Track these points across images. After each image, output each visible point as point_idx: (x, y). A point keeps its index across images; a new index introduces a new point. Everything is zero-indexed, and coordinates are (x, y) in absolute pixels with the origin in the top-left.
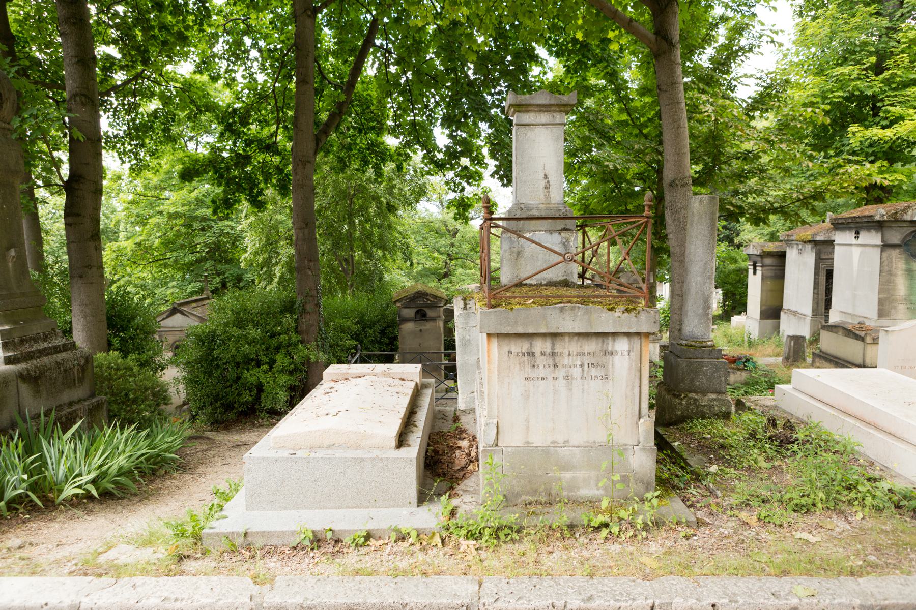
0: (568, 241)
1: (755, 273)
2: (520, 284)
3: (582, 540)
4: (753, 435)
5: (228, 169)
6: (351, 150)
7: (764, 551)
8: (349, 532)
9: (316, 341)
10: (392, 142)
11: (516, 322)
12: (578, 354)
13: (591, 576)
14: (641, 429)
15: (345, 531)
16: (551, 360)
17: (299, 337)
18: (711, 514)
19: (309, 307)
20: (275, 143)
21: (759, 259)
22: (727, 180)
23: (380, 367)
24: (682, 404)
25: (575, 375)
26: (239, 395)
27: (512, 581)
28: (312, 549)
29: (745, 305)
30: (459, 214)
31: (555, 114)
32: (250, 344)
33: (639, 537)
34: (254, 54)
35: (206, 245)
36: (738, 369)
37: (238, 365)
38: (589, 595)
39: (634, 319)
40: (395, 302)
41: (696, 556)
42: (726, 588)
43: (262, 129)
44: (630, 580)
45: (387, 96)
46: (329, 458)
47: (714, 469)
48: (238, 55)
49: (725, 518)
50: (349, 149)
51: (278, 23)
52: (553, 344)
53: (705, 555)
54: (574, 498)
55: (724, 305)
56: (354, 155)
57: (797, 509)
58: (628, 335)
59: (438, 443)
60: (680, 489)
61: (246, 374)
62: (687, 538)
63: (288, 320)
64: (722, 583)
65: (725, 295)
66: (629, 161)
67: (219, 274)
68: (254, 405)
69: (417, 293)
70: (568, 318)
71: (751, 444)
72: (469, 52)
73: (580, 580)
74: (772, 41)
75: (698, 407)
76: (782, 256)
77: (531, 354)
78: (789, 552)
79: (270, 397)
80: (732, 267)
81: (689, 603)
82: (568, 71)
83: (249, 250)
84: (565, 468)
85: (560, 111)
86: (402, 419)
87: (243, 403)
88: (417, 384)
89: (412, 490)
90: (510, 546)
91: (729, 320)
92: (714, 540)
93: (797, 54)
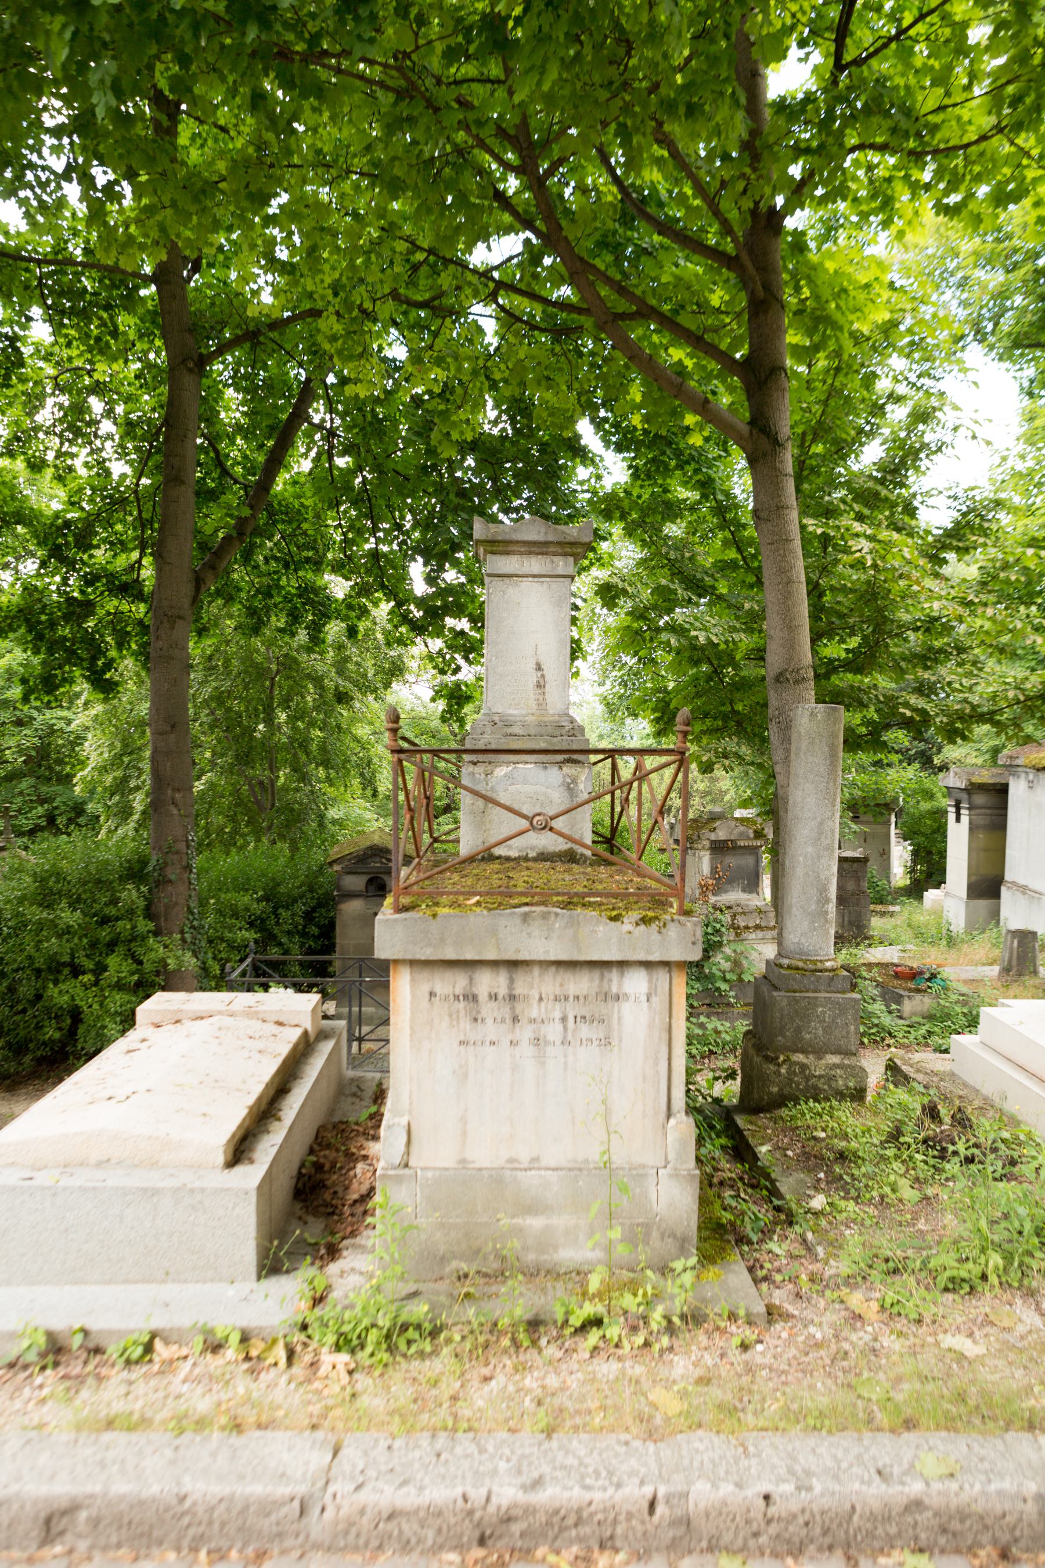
0: (574, 781)
1: (958, 820)
2: (487, 857)
3: (552, 1351)
4: (895, 1136)
5: (52, 624)
6: (271, 597)
7: (881, 1375)
8: (122, 1334)
9: (182, 932)
10: (339, 587)
11: (442, 940)
12: (556, 999)
13: (549, 1432)
14: (670, 1138)
15: (110, 1333)
16: (507, 1009)
17: (151, 926)
18: (798, 1296)
19: (172, 874)
20: (137, 580)
21: (964, 796)
22: (903, 664)
23: (243, 999)
24: (780, 1074)
25: (551, 1038)
26: (39, 1027)
27: (398, 1444)
28: (43, 1368)
29: (943, 871)
30: (450, 712)
31: (556, 559)
32: (59, 936)
33: (656, 1347)
34: (107, 427)
35: (20, 751)
36: (918, 991)
37: (38, 972)
38: (535, 1475)
39: (655, 937)
40: (331, 864)
41: (755, 1388)
42: (795, 1459)
43: (115, 556)
44: (619, 1442)
45: (330, 508)
46: (94, 1189)
47: (818, 1202)
48: (79, 429)
49: (822, 1303)
50: (267, 593)
51: (147, 377)
52: (512, 981)
53: (771, 1384)
54: (549, 1266)
55: (913, 871)
56: (275, 605)
57: (953, 1286)
58: (647, 965)
59: (328, 1146)
60: (750, 1243)
61: (52, 990)
62: (744, 1347)
63: (131, 894)
64: (790, 1448)
65: (915, 853)
66: (733, 629)
67: (42, 801)
68: (65, 1045)
69: (371, 848)
70: (536, 933)
71: (890, 1152)
72: (445, 443)
73: (528, 1440)
74: (974, 437)
75: (807, 1079)
76: (1002, 790)
77: (471, 998)
78: (924, 1379)
79: (93, 1033)
80: (925, 806)
81: (722, 1492)
82: (635, 476)
83: (92, 764)
84: (532, 1208)
85: (565, 554)
86: (251, 1108)
87: (44, 1043)
88: (306, 1033)
89: (248, 1253)
90: (415, 1364)
91: (920, 898)
92: (793, 1351)
93: (1023, 457)
